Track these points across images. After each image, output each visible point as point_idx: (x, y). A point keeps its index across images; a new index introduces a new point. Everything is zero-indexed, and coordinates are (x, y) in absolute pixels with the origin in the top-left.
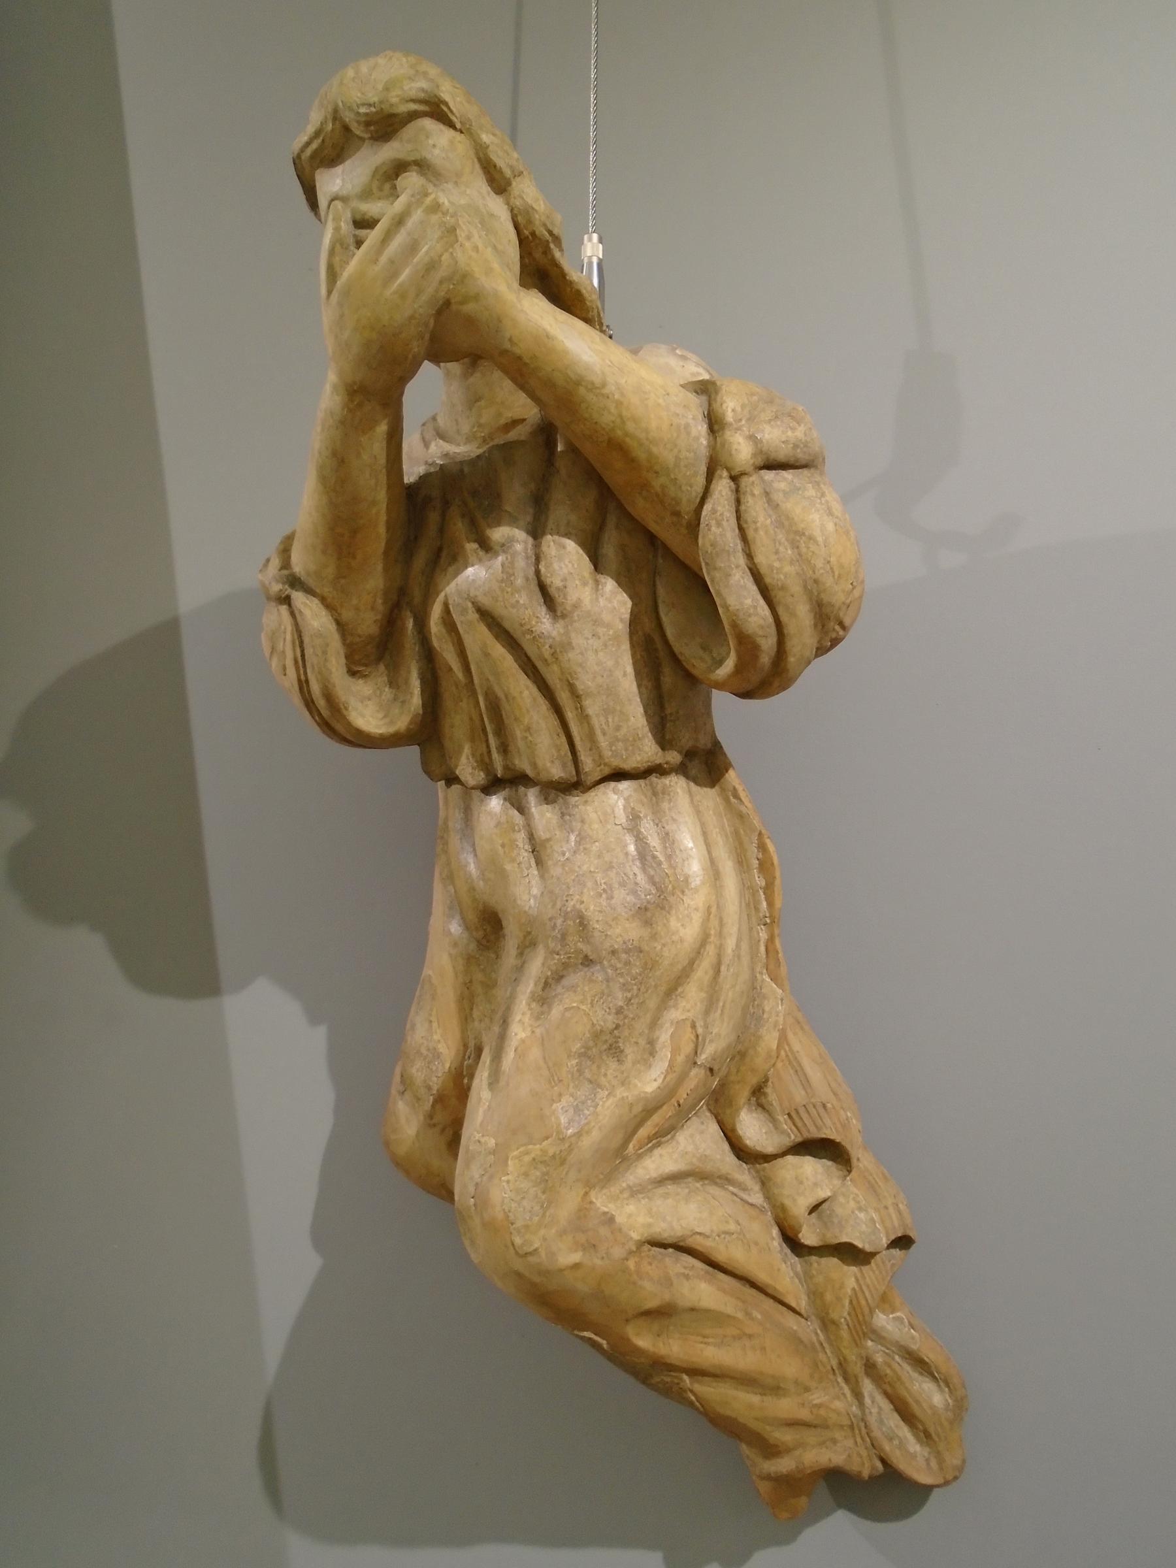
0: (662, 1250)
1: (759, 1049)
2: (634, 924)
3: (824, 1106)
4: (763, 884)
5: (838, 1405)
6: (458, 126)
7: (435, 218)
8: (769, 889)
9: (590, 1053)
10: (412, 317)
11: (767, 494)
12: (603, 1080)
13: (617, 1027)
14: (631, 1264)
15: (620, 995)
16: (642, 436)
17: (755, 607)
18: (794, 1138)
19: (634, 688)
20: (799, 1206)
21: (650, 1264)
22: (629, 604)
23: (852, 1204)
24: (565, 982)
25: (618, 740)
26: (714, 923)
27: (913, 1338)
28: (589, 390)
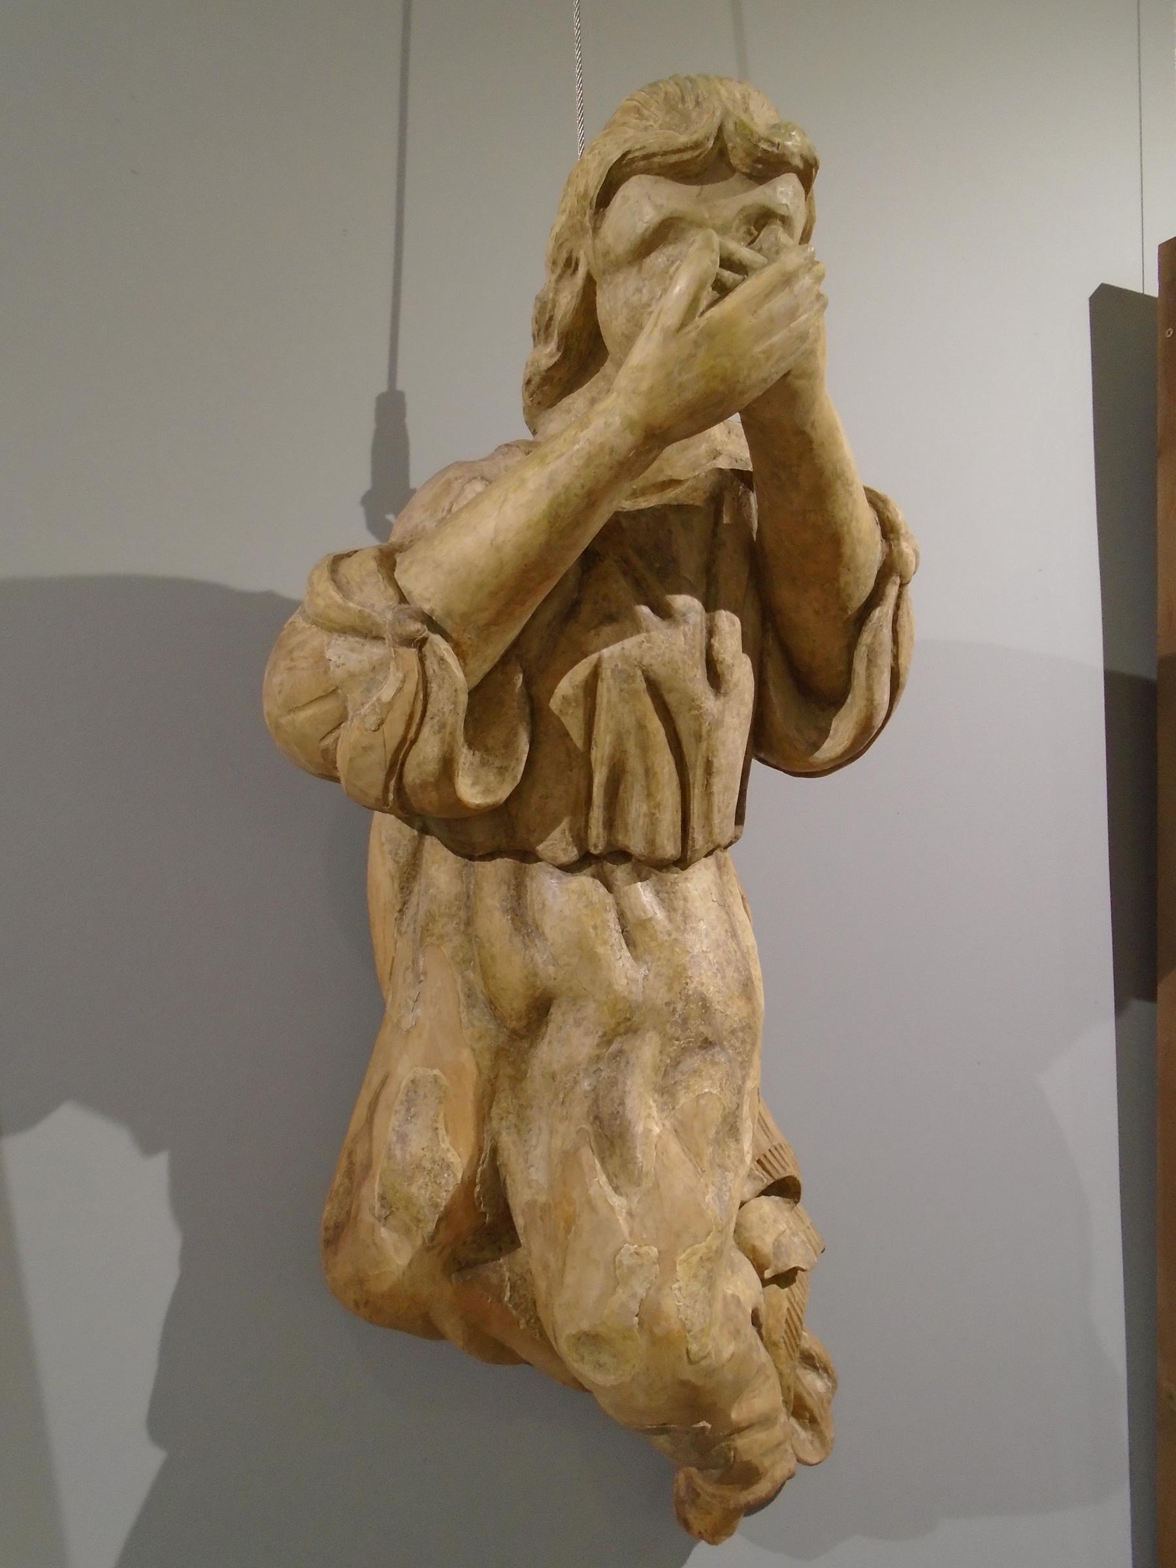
12: (728, 1162)
24: (681, 1067)
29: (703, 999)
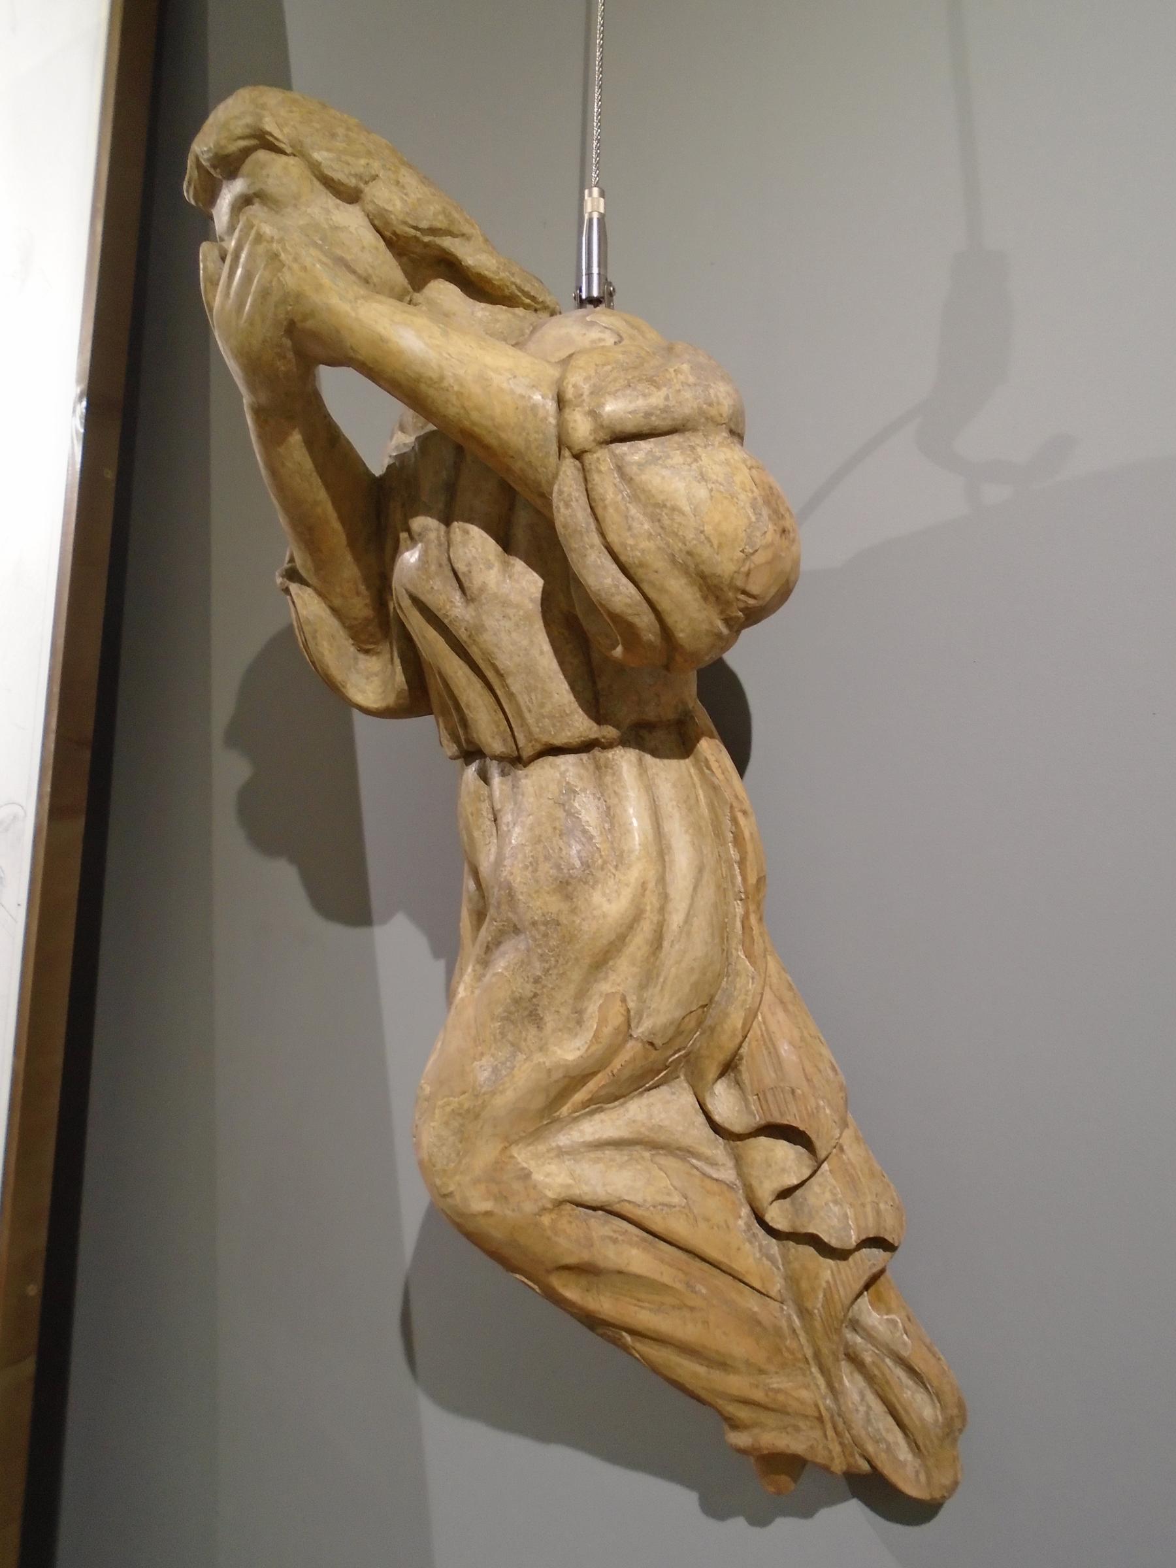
0: (590, 1212)
1: (726, 1027)
2: (554, 898)
3: (793, 1092)
4: (738, 858)
5: (804, 1394)
6: (289, 150)
7: (261, 249)
8: (742, 863)
9: (513, 1017)
10: (264, 341)
11: (620, 469)
13: (535, 995)
14: (546, 1220)
15: (537, 965)
16: (489, 423)
17: (617, 587)
18: (758, 1120)
19: (555, 665)
20: (766, 1189)
21: (570, 1222)
22: (540, 582)
23: (828, 1196)
25: (544, 717)
26: (651, 901)
27: (905, 1344)
28: (430, 386)
29: (510, 888)
